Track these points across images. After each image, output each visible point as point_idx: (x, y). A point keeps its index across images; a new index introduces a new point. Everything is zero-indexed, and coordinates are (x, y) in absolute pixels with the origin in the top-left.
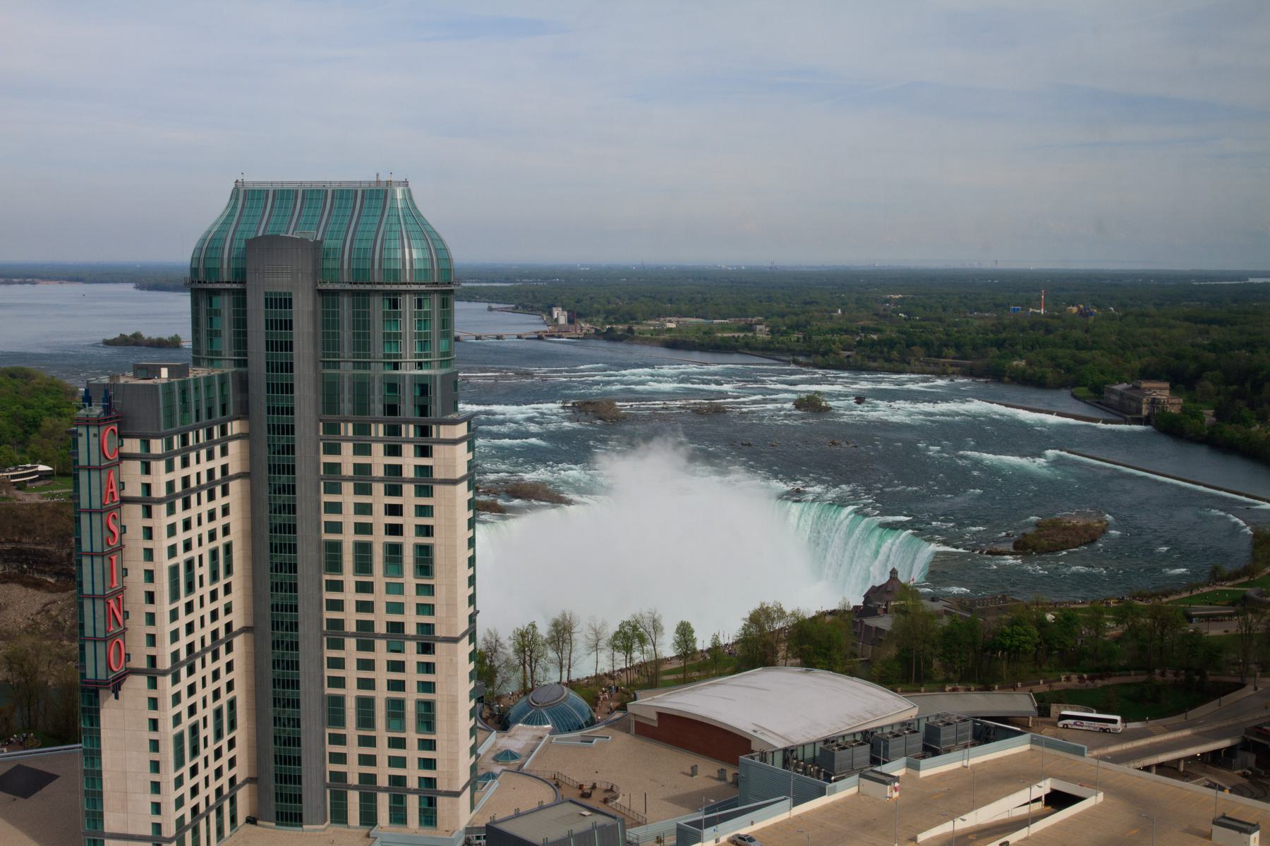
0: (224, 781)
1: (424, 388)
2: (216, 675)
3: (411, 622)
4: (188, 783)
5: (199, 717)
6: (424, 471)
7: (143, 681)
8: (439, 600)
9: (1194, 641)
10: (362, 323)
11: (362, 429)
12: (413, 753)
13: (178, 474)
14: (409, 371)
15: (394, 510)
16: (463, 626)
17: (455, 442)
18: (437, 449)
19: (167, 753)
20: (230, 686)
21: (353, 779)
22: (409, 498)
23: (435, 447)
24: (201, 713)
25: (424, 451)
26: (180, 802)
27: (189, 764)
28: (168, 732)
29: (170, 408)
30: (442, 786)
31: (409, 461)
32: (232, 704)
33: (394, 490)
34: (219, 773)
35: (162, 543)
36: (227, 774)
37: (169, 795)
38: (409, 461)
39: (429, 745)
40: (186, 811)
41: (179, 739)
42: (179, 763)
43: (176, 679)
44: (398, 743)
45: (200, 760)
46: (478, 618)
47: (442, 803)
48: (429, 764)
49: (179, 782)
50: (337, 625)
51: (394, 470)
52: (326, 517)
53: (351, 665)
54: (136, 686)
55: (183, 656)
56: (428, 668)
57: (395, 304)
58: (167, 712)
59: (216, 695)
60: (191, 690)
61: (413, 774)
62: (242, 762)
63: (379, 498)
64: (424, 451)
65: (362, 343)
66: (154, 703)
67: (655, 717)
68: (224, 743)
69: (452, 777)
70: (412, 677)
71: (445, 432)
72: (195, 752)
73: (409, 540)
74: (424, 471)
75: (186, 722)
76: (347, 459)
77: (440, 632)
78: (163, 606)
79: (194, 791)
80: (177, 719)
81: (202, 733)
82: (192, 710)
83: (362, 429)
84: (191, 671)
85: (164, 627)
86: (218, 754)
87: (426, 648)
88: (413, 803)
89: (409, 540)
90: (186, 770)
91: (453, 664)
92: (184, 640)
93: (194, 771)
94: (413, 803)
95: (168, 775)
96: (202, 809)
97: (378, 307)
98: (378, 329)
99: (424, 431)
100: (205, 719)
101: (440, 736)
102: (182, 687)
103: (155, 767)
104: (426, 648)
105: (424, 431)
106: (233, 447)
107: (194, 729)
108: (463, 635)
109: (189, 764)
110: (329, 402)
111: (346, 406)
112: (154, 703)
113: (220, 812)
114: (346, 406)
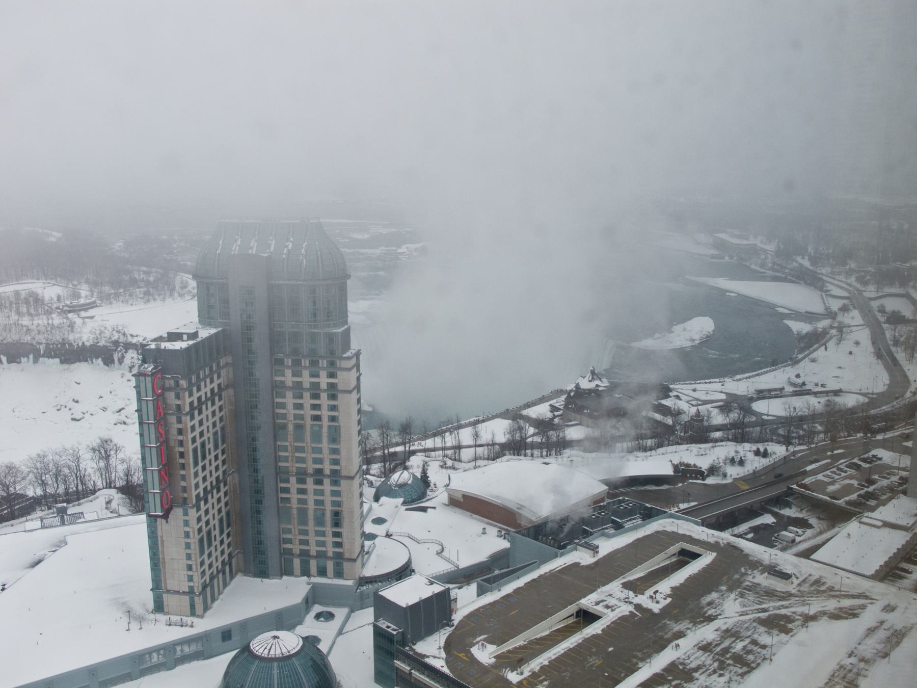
2: (214, 413)
3: (327, 468)
4: (201, 475)
5: (205, 438)
6: (332, 386)
8: (345, 539)
9: (763, 420)
13: (196, 395)
16: (354, 383)
17: (350, 370)
19: (195, 546)
23: (339, 373)
25: (332, 375)
26: (197, 486)
27: (201, 465)
33: (316, 396)
39: (335, 451)
40: (201, 490)
41: (195, 451)
42: (196, 463)
43: (192, 418)
45: (207, 462)
46: (361, 377)
47: (346, 565)
49: (196, 475)
55: (196, 404)
56: (333, 408)
60: (201, 423)
66: (186, 523)
67: (460, 496)
72: (204, 457)
74: (332, 386)
75: (199, 441)
79: (205, 479)
80: (194, 440)
82: (202, 434)
84: (200, 413)
87: (335, 483)
89: (329, 508)
90: (199, 468)
93: (204, 468)
96: (209, 488)
99: (332, 364)
100: (209, 438)
102: (196, 422)
103: (189, 557)
104: (333, 397)
105: (332, 364)
106: (223, 372)
107: (203, 445)
108: (354, 389)
109: (201, 465)
112: (186, 523)
113: (224, 573)
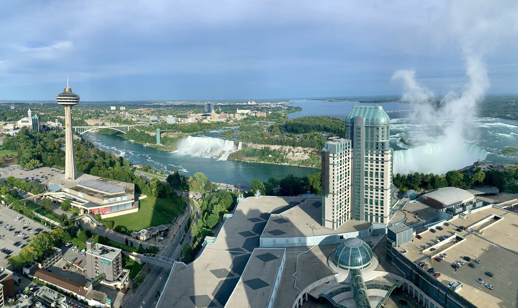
0: (346, 212)
1: (383, 144)
5: (342, 201)
7: (332, 195)
8: (384, 182)
10: (372, 132)
11: (372, 151)
12: (380, 182)
14: (380, 141)
15: (377, 184)
18: (385, 155)
20: (348, 168)
21: (369, 213)
22: (380, 164)
24: (342, 200)
25: (383, 156)
28: (336, 204)
29: (338, 148)
30: (384, 216)
31: (380, 157)
32: (348, 199)
34: (345, 183)
35: (336, 172)
36: (347, 211)
37: (335, 215)
38: (380, 157)
44: (377, 180)
48: (382, 184)
50: (367, 186)
51: (377, 159)
52: (365, 167)
53: (369, 193)
54: (330, 196)
57: (378, 129)
58: (336, 201)
59: (346, 169)
61: (380, 213)
62: (350, 182)
63: (374, 164)
64: (383, 156)
65: (372, 136)
68: (346, 205)
69: (386, 215)
70: (380, 168)
71: (386, 152)
73: (380, 171)
76: (369, 157)
77: (385, 188)
78: (336, 183)
81: (342, 176)
83: (372, 151)
85: (336, 186)
86: (346, 180)
87: (382, 191)
88: (379, 218)
90: (339, 211)
91: (387, 194)
92: (339, 188)
93: (341, 183)
94: (379, 218)
95: (335, 211)
97: (375, 129)
98: (375, 133)
99: (383, 152)
101: (384, 207)
104: (382, 191)
105: (383, 152)
109: (339, 209)
110: (367, 146)
111: (369, 147)
114: (369, 147)
